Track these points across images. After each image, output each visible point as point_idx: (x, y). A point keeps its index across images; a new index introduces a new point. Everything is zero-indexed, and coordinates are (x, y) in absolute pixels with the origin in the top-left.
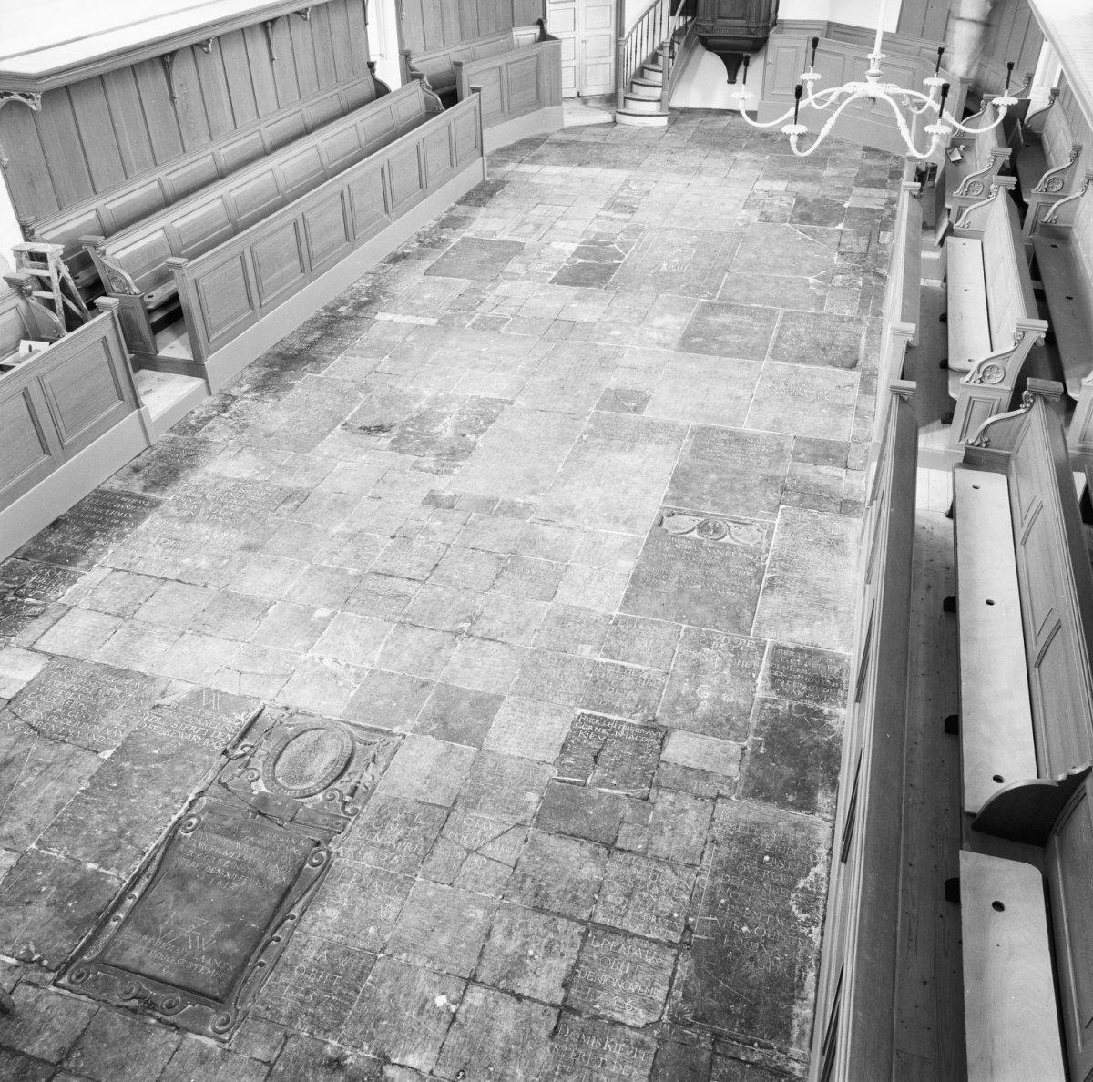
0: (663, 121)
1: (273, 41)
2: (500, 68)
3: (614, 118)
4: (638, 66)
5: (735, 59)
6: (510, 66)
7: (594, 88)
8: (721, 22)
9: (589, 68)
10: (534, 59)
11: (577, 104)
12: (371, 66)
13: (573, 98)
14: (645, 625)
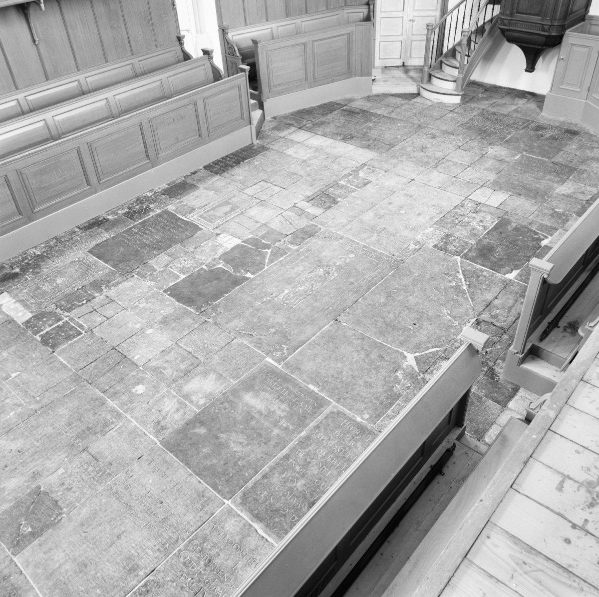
0: (457, 100)
1: (32, 25)
2: (304, 44)
3: (419, 90)
4: (451, 46)
5: (534, 51)
6: (316, 43)
7: (417, 60)
8: (519, 16)
9: (414, 43)
10: (346, 37)
11: (399, 73)
12: (180, 39)
13: (398, 67)
14: (356, 434)
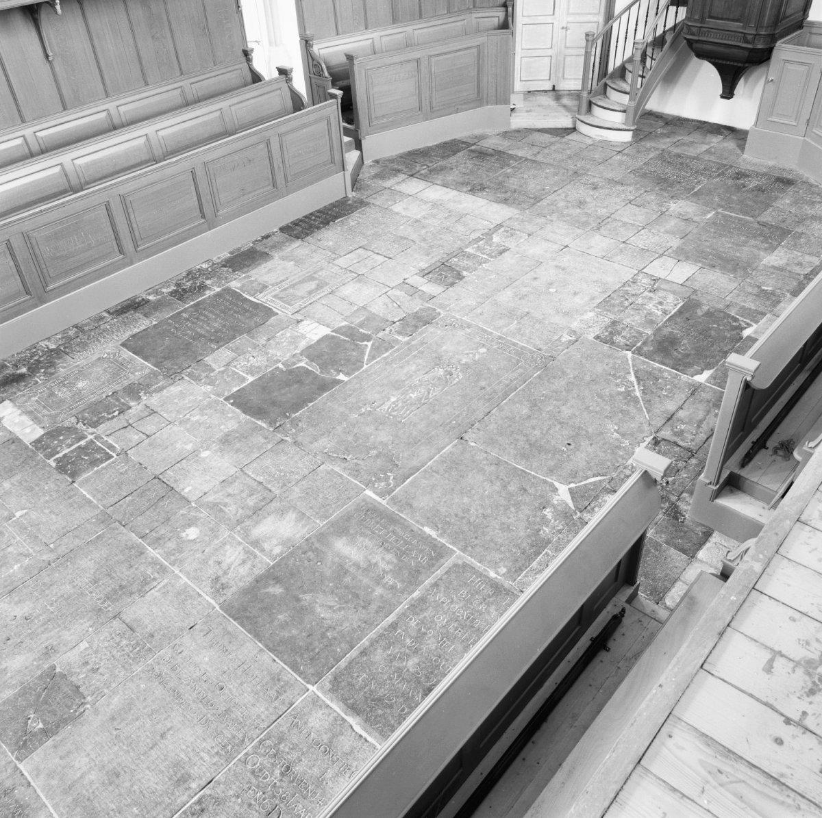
0: (627, 137)
1: (44, 34)
2: (418, 61)
3: (575, 123)
4: (618, 63)
5: (733, 70)
6: (433, 59)
7: (573, 82)
8: (712, 23)
9: (568, 59)
10: (474, 50)
11: (548, 100)
12: (246, 54)
13: (546, 91)
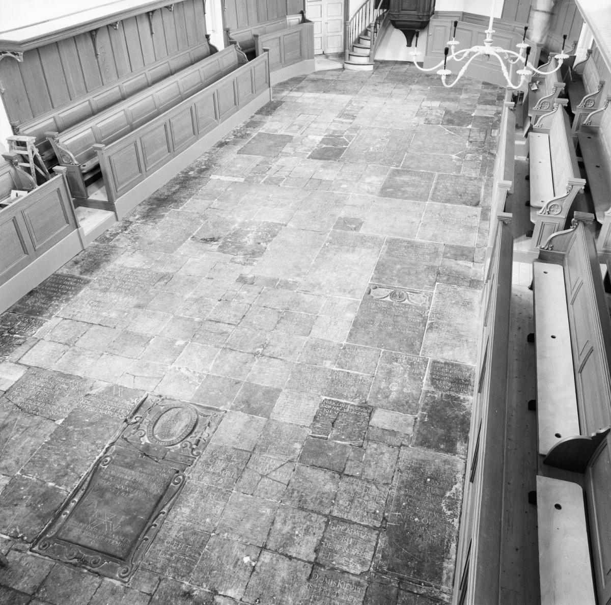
0: (371, 68)
1: (153, 23)
2: (279, 38)
3: (343, 66)
4: (357, 37)
5: (411, 33)
6: (285, 37)
7: (332, 49)
8: (403, 12)
9: (329, 38)
10: (298, 33)
11: (322, 58)
12: (207, 37)
13: (320, 55)
14: (360, 350)
